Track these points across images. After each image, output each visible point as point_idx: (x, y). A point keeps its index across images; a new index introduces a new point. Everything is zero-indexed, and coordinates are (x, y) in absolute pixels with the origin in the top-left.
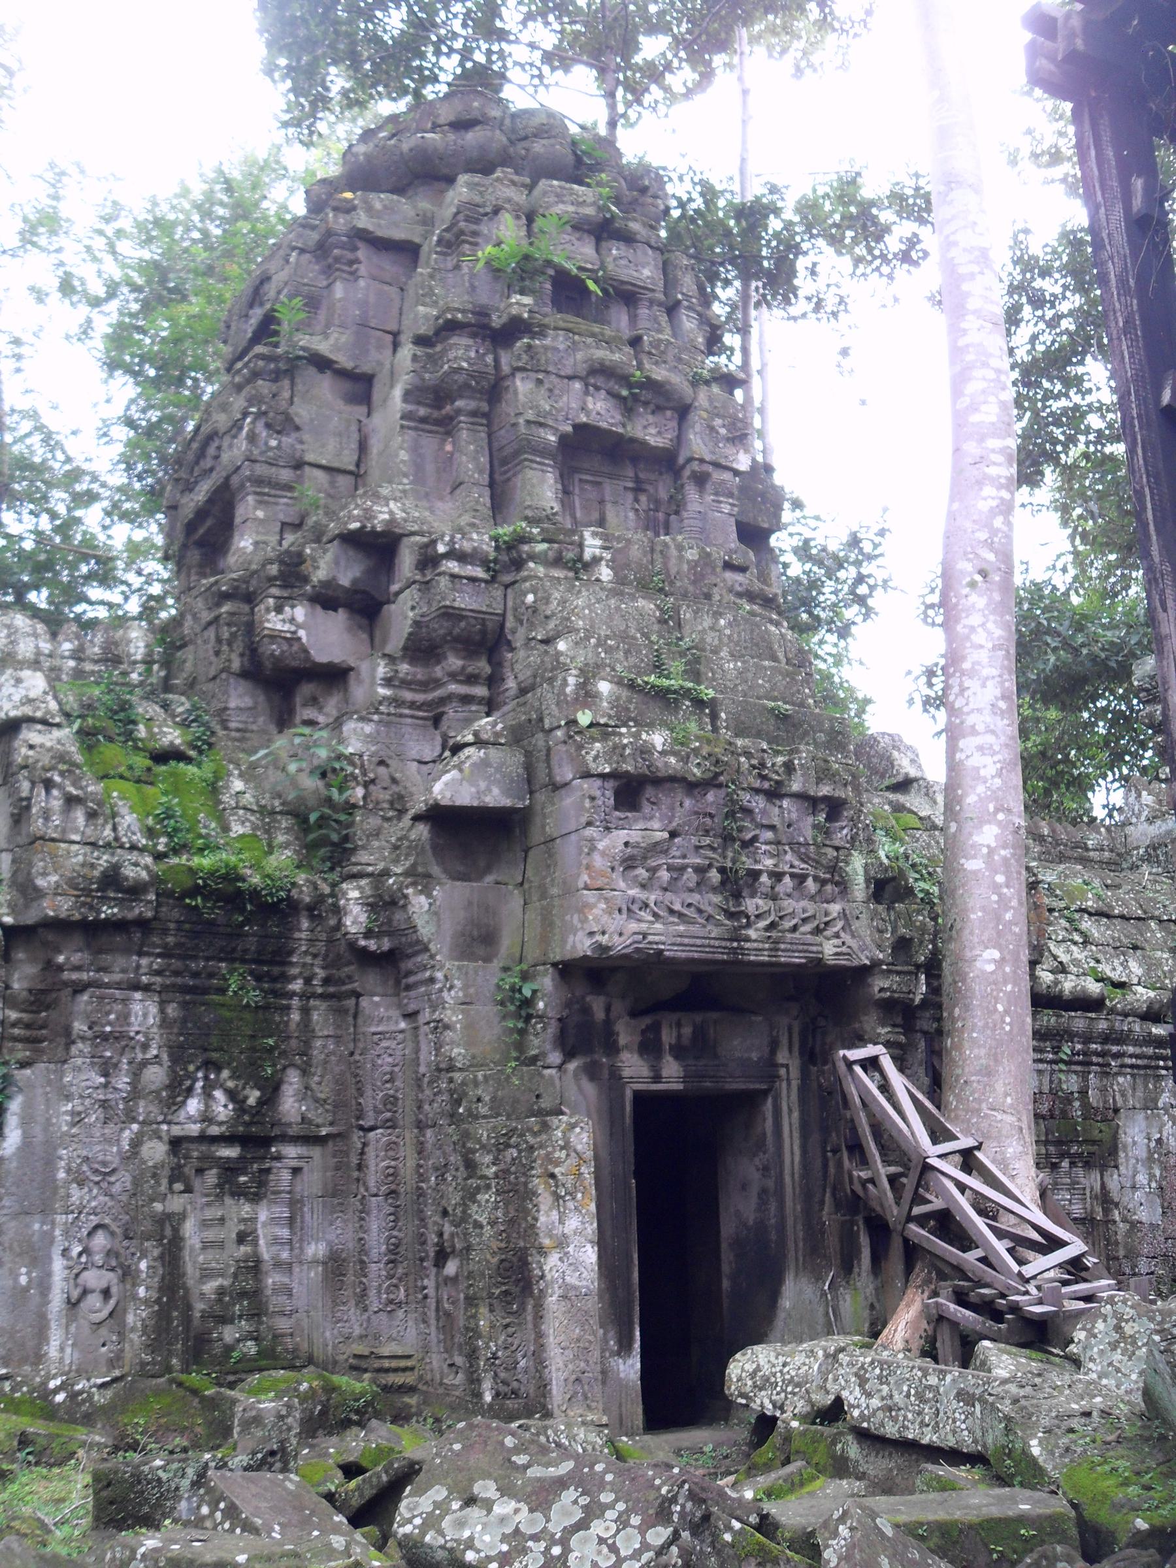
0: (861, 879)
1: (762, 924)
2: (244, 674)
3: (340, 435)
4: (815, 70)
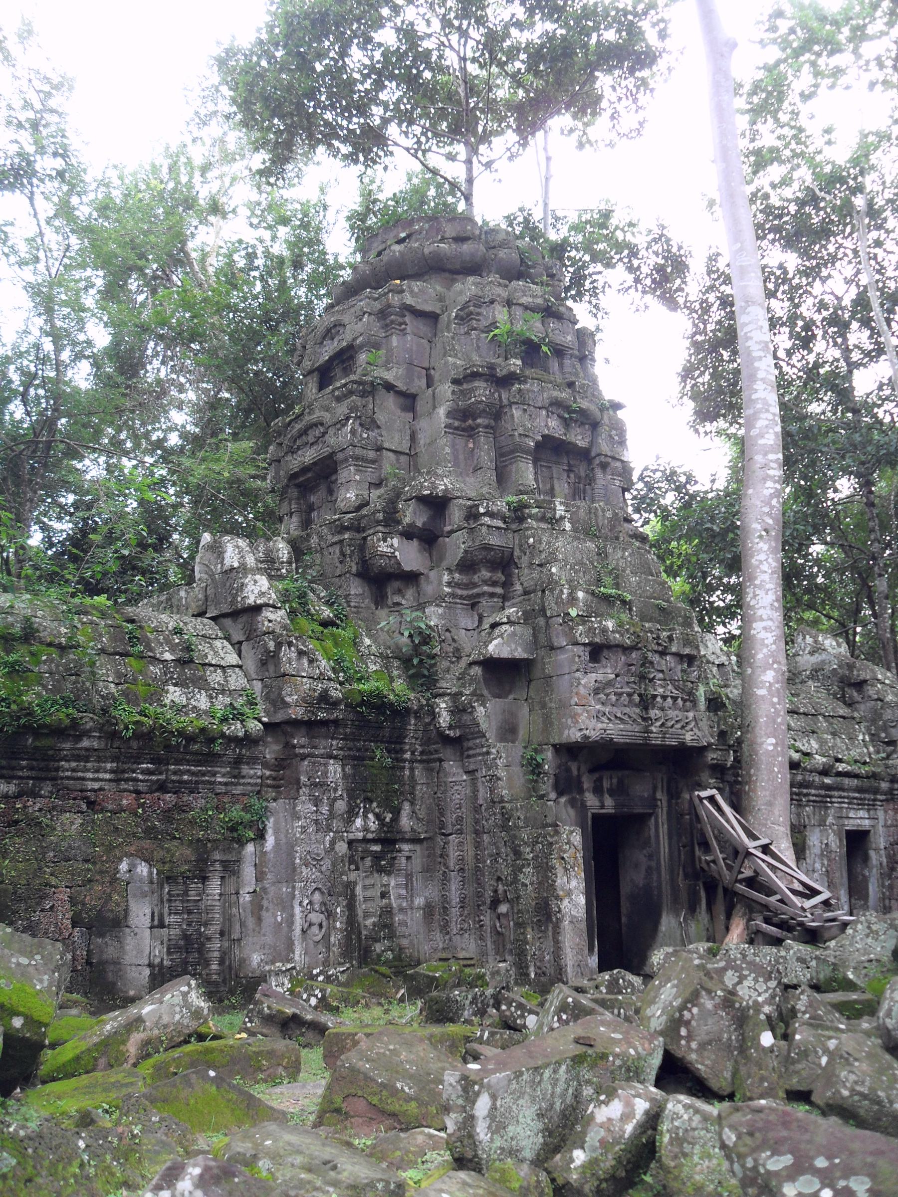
0: (703, 699)
1: (658, 724)
2: (359, 575)
3: (401, 431)
4: (592, 145)
